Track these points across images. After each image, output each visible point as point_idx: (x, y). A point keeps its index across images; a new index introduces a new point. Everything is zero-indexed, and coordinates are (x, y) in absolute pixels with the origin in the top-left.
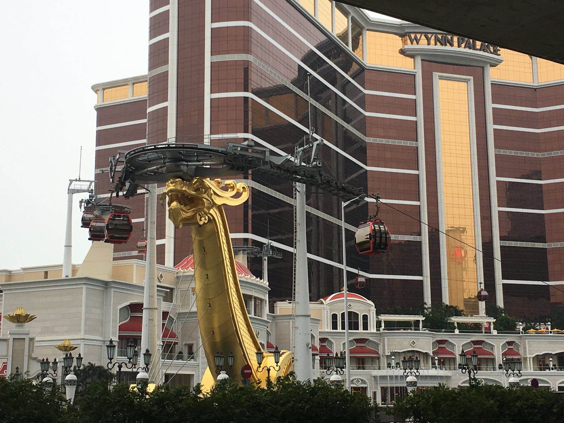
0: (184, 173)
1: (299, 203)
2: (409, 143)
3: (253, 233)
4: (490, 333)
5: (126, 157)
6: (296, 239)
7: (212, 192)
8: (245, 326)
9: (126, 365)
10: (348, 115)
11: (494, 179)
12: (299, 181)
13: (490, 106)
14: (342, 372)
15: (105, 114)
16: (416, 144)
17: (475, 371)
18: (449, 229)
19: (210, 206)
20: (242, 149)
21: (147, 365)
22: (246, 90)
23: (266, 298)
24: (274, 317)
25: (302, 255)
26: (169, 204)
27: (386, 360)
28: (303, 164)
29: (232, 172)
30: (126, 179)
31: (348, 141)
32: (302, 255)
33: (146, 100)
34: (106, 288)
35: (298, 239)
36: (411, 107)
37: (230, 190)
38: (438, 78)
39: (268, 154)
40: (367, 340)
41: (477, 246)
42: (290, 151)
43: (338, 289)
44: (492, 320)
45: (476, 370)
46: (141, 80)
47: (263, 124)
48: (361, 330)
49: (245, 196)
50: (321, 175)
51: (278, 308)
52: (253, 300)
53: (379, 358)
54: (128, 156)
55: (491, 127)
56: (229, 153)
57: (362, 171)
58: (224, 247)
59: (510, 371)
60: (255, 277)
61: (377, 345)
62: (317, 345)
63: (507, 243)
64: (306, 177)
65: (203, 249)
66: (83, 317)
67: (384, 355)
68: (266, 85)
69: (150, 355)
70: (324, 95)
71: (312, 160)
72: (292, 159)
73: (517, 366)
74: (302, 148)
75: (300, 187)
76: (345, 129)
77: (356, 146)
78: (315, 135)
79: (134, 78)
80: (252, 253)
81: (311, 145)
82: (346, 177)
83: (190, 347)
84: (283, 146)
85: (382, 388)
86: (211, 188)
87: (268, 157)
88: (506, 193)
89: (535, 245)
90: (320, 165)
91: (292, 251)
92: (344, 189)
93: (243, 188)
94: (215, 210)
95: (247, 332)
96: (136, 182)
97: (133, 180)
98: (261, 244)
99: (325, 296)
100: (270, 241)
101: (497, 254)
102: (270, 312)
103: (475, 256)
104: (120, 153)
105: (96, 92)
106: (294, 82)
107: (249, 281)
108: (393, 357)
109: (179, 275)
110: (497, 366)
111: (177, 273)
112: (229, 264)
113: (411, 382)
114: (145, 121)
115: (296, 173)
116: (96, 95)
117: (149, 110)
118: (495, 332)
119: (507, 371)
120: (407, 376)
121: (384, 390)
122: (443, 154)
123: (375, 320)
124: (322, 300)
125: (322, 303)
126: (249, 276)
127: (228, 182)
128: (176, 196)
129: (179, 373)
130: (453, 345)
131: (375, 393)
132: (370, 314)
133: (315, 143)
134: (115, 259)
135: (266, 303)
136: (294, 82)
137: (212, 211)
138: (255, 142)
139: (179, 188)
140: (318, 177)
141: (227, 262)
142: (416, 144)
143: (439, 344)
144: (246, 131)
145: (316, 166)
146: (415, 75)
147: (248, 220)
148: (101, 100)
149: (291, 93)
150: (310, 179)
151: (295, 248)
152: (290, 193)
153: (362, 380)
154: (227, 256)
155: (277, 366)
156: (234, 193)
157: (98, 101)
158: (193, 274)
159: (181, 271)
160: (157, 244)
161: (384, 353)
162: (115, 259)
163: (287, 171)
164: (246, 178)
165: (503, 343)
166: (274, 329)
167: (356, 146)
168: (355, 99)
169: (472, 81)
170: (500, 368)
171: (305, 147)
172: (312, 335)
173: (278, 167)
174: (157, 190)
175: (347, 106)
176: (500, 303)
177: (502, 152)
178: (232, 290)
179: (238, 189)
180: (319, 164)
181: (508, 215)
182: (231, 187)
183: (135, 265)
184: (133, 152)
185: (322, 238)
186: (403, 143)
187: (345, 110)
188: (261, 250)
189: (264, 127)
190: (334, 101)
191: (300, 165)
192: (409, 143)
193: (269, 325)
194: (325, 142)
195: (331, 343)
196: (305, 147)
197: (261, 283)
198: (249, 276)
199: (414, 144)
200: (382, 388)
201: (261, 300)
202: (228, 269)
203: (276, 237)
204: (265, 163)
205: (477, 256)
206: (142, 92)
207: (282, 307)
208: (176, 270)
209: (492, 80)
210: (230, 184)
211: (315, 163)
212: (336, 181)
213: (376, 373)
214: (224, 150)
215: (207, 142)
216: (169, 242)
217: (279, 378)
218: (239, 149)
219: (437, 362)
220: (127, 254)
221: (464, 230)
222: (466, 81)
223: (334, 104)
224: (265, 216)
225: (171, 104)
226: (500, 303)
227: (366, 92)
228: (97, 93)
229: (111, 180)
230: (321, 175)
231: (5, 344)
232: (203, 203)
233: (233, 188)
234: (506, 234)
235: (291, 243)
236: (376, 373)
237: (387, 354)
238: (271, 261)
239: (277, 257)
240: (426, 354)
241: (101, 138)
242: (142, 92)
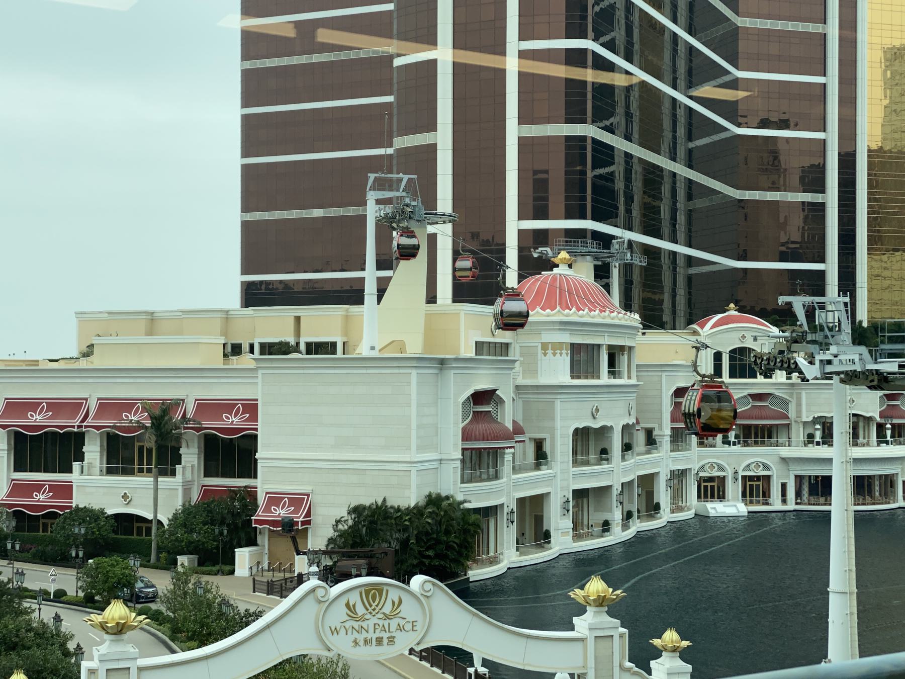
2: (811, 28)
3: (594, 219)
27: (801, 429)
34: (441, 369)
61: (786, 402)
66: (414, 425)
67: (798, 419)
85: (796, 476)
88: (885, 72)
107: (616, 322)
121: (799, 479)
125: (695, 333)
131: (784, 486)
143: (888, 400)
147: (585, 197)
153: (764, 464)
161: (799, 415)
183: (462, 314)
186: (801, 27)
192: (811, 28)
198: (607, 312)
200: (796, 476)
213: (785, 452)
219: (889, 433)
231: (579, 645)
236: (785, 452)
237: (804, 419)
240: (869, 420)
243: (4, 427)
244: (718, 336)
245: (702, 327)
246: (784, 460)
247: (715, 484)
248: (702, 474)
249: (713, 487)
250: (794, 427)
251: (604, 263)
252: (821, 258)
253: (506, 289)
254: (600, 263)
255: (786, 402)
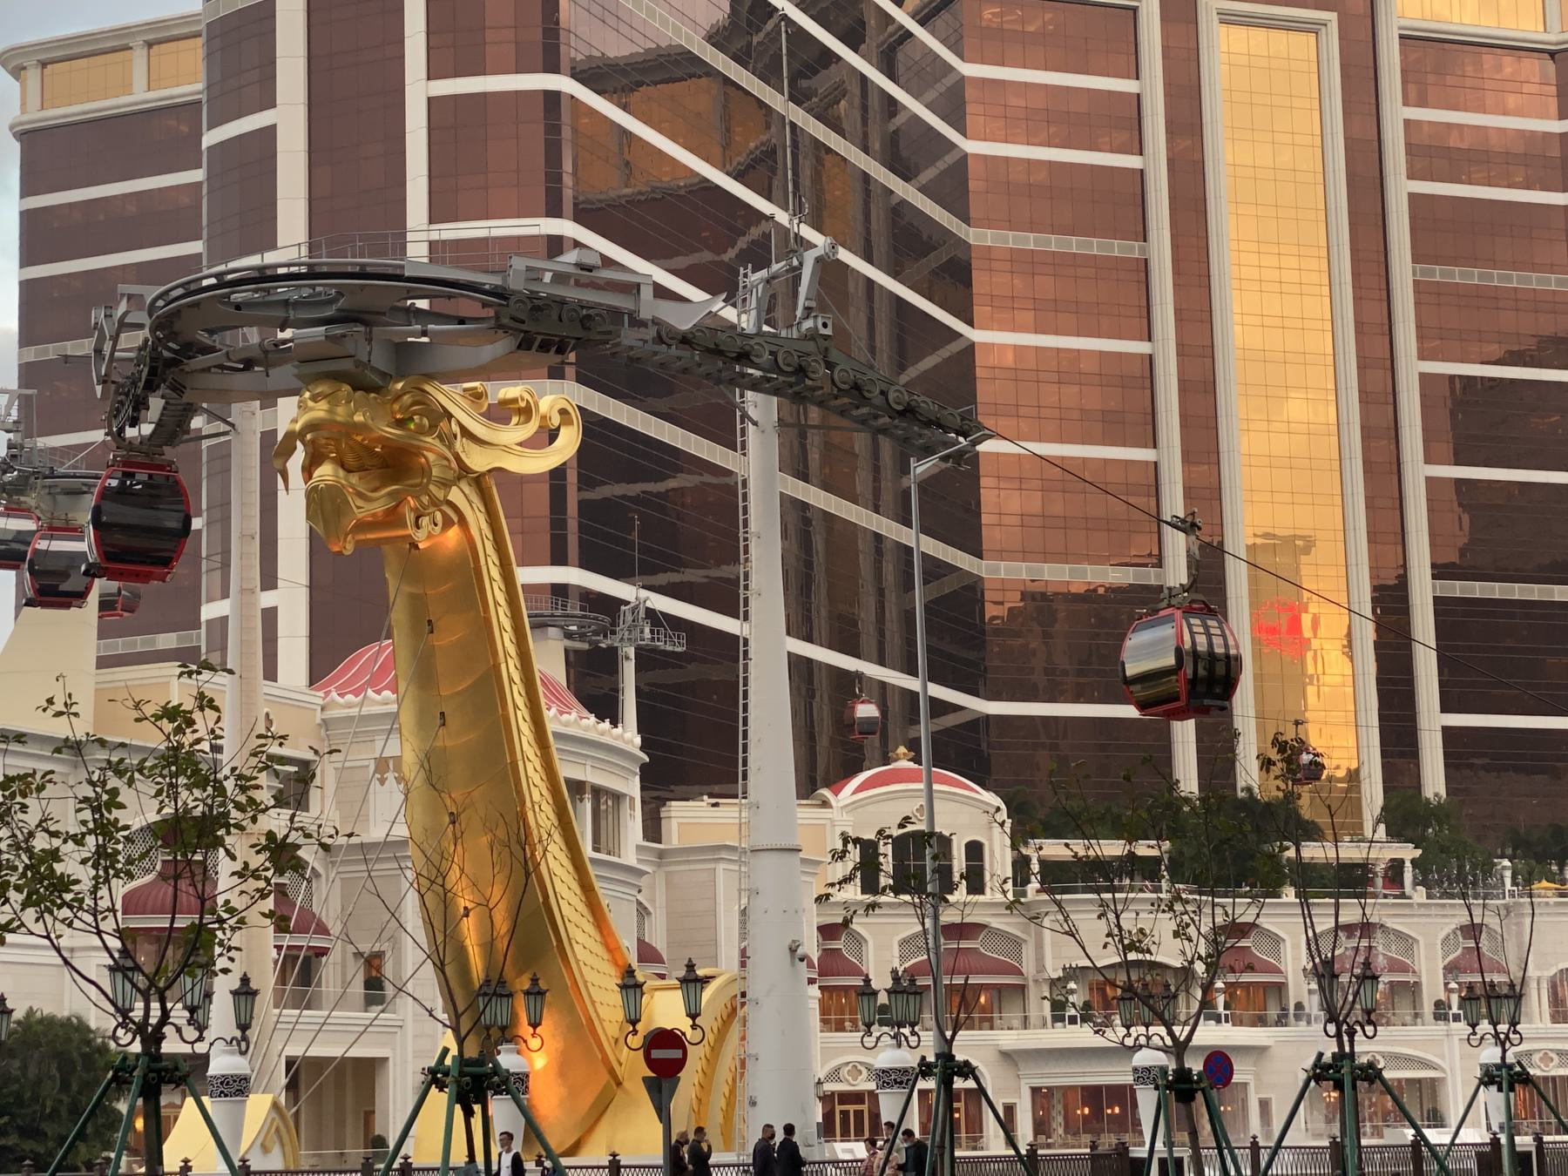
0: (358, 364)
1: (757, 464)
2: (1117, 248)
3: (586, 564)
4: (1403, 896)
5: (152, 309)
6: (746, 587)
7: (455, 428)
8: (575, 886)
9: (179, 1030)
10: (907, 150)
11: (1412, 367)
12: (756, 386)
13: (1396, 113)
14: (913, 1040)
15: (47, 154)
16: (1143, 250)
17: (1369, 1029)
18: (1259, 541)
19: (450, 475)
20: (559, 278)
21: (244, 1027)
22: (552, 67)
23: (632, 787)
24: (661, 855)
25: (768, 640)
26: (308, 471)
28: (766, 328)
29: (531, 356)
30: (150, 387)
31: (907, 243)
32: (768, 640)
33: (199, 102)
35: (753, 585)
36: (1122, 124)
37: (515, 420)
38: (1216, 18)
39: (647, 293)
40: (983, 927)
41: (1355, 598)
42: (721, 282)
43: (877, 755)
44: (1408, 852)
45: (1370, 1022)
46: (176, 32)
47: (609, 185)
48: (960, 895)
49: (568, 442)
50: (830, 366)
51: (674, 823)
52: (588, 796)
53: (1022, 989)
54: (160, 303)
55: (1401, 188)
56: (514, 292)
57: (954, 347)
58: (501, 617)
59: (1485, 1026)
60: (593, 718)
61: (1016, 943)
62: (812, 947)
63: (1458, 589)
64: (781, 372)
65: (424, 625)
67: (1040, 977)
68: (617, 48)
69: (255, 993)
70: (822, 82)
71: (799, 313)
72: (730, 314)
73: (1507, 1008)
74: (763, 273)
75: (760, 408)
76: (894, 201)
77: (933, 261)
78: (807, 232)
79: (152, 26)
80: (582, 637)
81: (795, 263)
82: (902, 368)
83: (373, 963)
84: (682, 262)
86: (450, 416)
87: (649, 307)
89: (1552, 593)
90: (828, 332)
91: (738, 633)
92: (909, 412)
93: (563, 412)
94: (467, 489)
95: (582, 908)
96: (188, 397)
97: (178, 388)
98: (608, 606)
99: (836, 779)
100: (644, 593)
101: (1424, 625)
102: (646, 837)
103: (1349, 635)
104: (130, 297)
105: (17, 72)
106: (717, 38)
108: (1072, 985)
109: (329, 714)
110: (1428, 1009)
111: (323, 709)
112: (516, 676)
113: (1148, 1069)
114: (198, 175)
115: (744, 357)
116: (15, 85)
117: (210, 138)
118: (1419, 895)
119: (1473, 1026)
120: (1137, 1047)
122: (1235, 284)
123: (1009, 856)
124: (825, 792)
125: (825, 804)
126: (574, 715)
127: (511, 390)
128: (320, 443)
129: (352, 1053)
130: (1276, 940)
132: (991, 840)
133: (809, 257)
134: (103, 663)
135: (632, 807)
136: (717, 38)
137: (455, 495)
138: (604, 258)
139: (341, 413)
140: (823, 371)
141: (511, 669)
142: (1143, 250)
144: (554, 211)
145: (812, 336)
146: (1135, 10)
147: (565, 521)
148: (34, 99)
149: (708, 74)
150: (792, 380)
151: (746, 618)
152: (724, 430)
154: (512, 649)
155: (694, 1027)
156: (532, 427)
157: (23, 104)
158: (394, 708)
159: (344, 704)
160: (227, 602)
161: (1041, 968)
162: (103, 663)
163: (717, 352)
164: (556, 373)
165: (1448, 930)
166: (661, 899)
167: (933, 261)
168: (931, 95)
169: (1334, 28)
170: (1437, 1017)
171: (775, 267)
172: (639, 903)
173: (685, 340)
174: (252, 420)
175: (899, 120)
176: (1434, 781)
177: (1438, 273)
178: (530, 767)
179: (543, 418)
180: (825, 325)
181: (1458, 491)
182: (520, 411)
184: (180, 291)
185: (827, 582)
187: (896, 132)
188: (614, 623)
189: (613, 194)
190: (857, 101)
191: (760, 333)
193: (643, 882)
194: (844, 255)
195: (859, 940)
196: (775, 267)
197: (616, 738)
199: (1134, 249)
200: (1035, 1091)
201: (617, 797)
202: (516, 695)
203: (662, 579)
204: (637, 323)
205: (1356, 635)
206: (187, 81)
207: (690, 818)
208: (317, 698)
209: (1404, 23)
210: (515, 401)
211: (808, 324)
212: (884, 387)
213: (1009, 1039)
214: (496, 280)
215: (417, 251)
216: (292, 602)
217: (938, 1056)
218: (548, 277)
220: (139, 643)
221: (1309, 545)
222: (1314, 28)
223: (857, 115)
224: (635, 512)
225: (289, 118)
226: (1434, 781)
227: (969, 70)
228: (17, 79)
229: (99, 389)
230: (830, 366)
232: (425, 471)
233: (526, 413)
234: (1454, 557)
235: (728, 599)
236: (1009, 1039)
238: (646, 659)
239: (669, 648)
241: (38, 237)
242: (187, 81)
243: (239, 47)
244: (871, 808)
245: (836, 793)
246: (1009, 1057)
247: (865, 1107)
248: (829, 1087)
249: (859, 1114)
250: (1033, 994)
251: (595, 649)
252: (1449, 733)
253: (663, 801)
254: (586, 646)
255: (1016, 943)
